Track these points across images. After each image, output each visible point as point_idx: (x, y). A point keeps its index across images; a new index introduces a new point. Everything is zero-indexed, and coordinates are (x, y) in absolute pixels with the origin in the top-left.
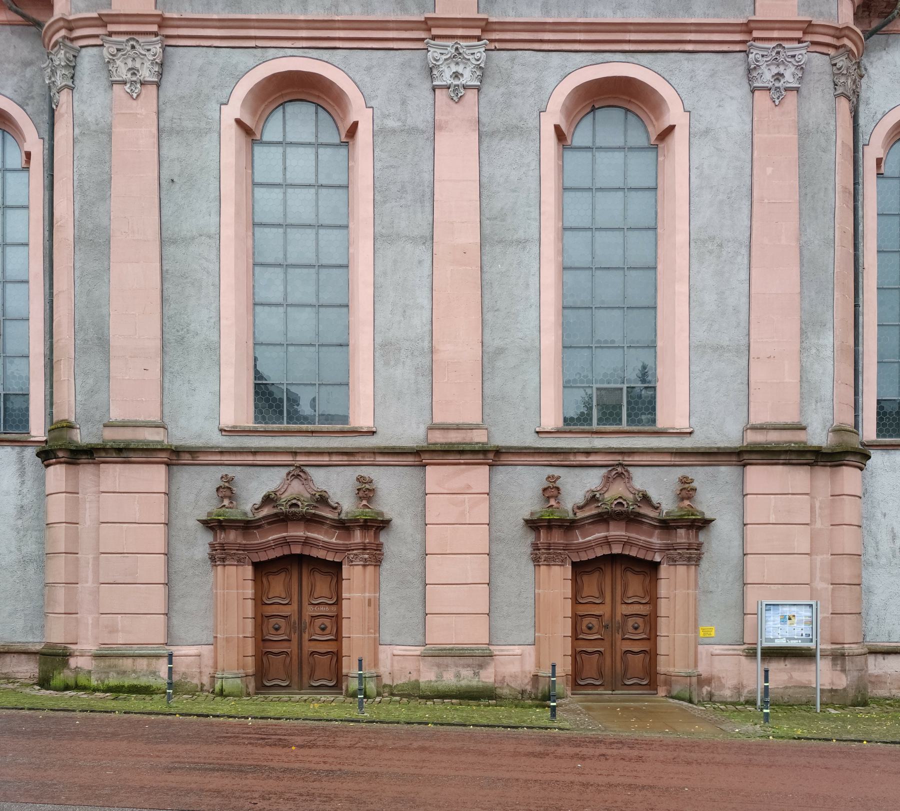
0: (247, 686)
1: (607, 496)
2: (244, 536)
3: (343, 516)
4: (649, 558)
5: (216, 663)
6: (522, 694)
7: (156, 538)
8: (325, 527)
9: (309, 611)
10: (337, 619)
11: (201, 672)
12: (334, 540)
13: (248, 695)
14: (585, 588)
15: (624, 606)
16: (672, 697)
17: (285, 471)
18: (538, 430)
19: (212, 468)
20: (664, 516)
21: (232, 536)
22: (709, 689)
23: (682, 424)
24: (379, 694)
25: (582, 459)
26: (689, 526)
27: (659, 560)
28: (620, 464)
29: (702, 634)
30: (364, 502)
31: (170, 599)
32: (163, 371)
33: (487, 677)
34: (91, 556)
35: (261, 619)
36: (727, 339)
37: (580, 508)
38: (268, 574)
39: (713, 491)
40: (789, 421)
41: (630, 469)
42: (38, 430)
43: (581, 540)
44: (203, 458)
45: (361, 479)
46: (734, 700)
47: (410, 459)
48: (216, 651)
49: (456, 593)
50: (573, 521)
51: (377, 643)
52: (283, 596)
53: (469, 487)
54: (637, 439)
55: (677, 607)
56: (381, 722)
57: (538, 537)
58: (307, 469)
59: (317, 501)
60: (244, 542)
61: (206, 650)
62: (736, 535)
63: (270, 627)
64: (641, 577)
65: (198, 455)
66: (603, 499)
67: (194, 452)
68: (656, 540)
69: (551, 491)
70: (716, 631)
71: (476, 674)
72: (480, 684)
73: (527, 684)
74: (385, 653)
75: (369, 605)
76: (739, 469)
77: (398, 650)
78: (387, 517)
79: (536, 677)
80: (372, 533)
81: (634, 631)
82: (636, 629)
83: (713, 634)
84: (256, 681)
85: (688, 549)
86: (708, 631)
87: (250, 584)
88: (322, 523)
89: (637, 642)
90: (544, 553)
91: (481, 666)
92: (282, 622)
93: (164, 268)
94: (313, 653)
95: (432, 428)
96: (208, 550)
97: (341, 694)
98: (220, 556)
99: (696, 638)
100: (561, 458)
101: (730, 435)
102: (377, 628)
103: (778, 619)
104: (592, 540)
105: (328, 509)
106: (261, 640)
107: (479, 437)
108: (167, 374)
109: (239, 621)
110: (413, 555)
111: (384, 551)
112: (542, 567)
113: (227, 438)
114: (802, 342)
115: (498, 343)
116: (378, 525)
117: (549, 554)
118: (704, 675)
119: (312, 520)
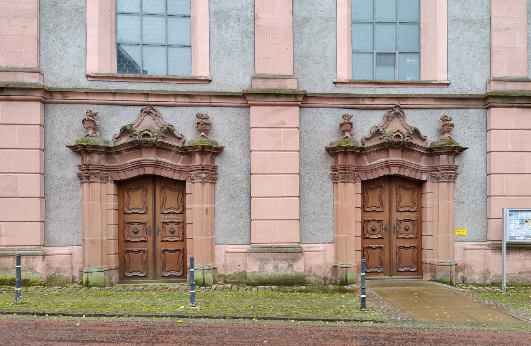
0: (110, 278)
1: (388, 131)
2: (107, 160)
3: (186, 145)
4: (418, 177)
6: (325, 280)
7: (33, 162)
8: (172, 154)
9: (161, 219)
10: (183, 224)
11: (72, 268)
12: (179, 164)
13: (112, 284)
14: (370, 200)
15: (398, 213)
16: (436, 281)
17: (139, 109)
18: (335, 81)
19: (80, 106)
20: (429, 146)
21: (96, 159)
22: (462, 274)
23: (442, 78)
24: (215, 282)
25: (368, 103)
27: (425, 179)
28: (398, 107)
29: (457, 234)
30: (203, 134)
31: (46, 210)
32: (40, 29)
33: (300, 268)
35: (123, 225)
36: (474, 15)
37: (367, 139)
38: (128, 190)
39: (466, 127)
41: (405, 111)
43: (368, 164)
44: (72, 98)
46: (482, 282)
47: (239, 101)
48: (83, 250)
49: (276, 202)
50: (363, 149)
51: (213, 243)
52: (141, 207)
53: (284, 123)
54: (409, 88)
55: (440, 214)
56: (209, 317)
57: (336, 161)
58: (157, 108)
59: (165, 133)
60: (107, 165)
61: (76, 250)
62: (482, 160)
63: (131, 231)
64: (411, 192)
65: (68, 95)
66: (385, 133)
67: (64, 93)
68: (423, 163)
69: (346, 126)
70: (467, 231)
71: (290, 266)
72: (294, 273)
73: (329, 273)
74: (220, 251)
75: (207, 213)
76: (484, 111)
78: (220, 145)
79: (335, 268)
80: (209, 157)
81: (405, 232)
82: (407, 230)
83: (465, 234)
84: (119, 273)
85: (448, 170)
86: (461, 231)
88: (170, 150)
89: (408, 240)
90: (341, 173)
91: (294, 260)
92: (140, 227)
94: (164, 251)
97: (186, 282)
98: (86, 174)
99: (454, 235)
100: (353, 102)
101: (477, 86)
102: (214, 232)
103: (518, 222)
104: (376, 164)
105: (174, 140)
106: (124, 242)
107: (291, 85)
108: (43, 31)
110: (241, 175)
111: (218, 172)
112: (339, 184)
113: (92, 83)
115: (305, 14)
116: (214, 151)
117: (346, 173)
119: (161, 148)
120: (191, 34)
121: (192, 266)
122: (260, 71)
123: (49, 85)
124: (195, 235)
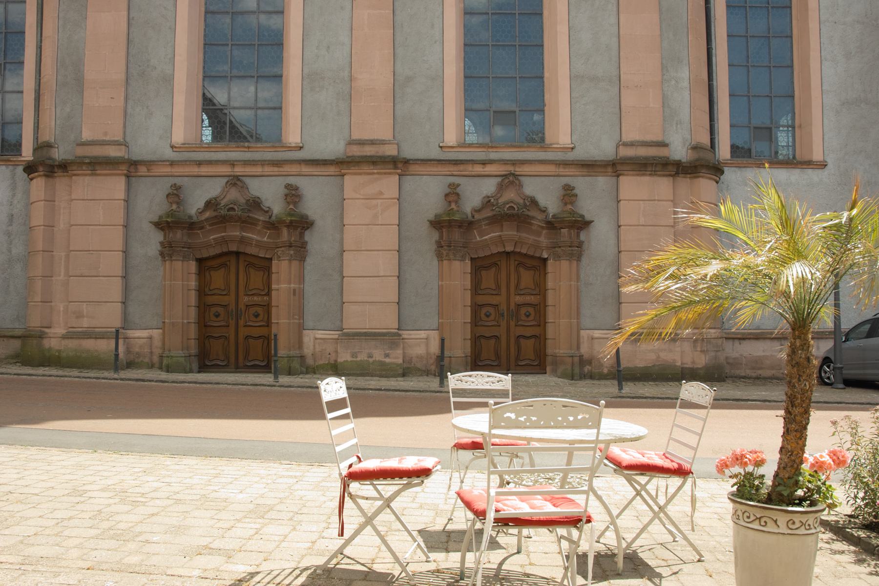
5: (164, 344)
10: (267, 307)
11: (151, 353)
22: (590, 368)
25: (478, 169)
26: (571, 226)
31: (126, 289)
32: (126, 99)
34: (63, 254)
37: (478, 211)
40: (655, 139)
42: (27, 153)
45: (288, 186)
47: (332, 170)
50: (471, 223)
51: (301, 328)
58: (244, 179)
61: (156, 333)
64: (532, 272)
66: (497, 203)
69: (453, 195)
74: (309, 337)
75: (294, 294)
77: (320, 334)
87: (193, 277)
93: (131, 17)
94: (247, 337)
95: (351, 143)
96: (160, 248)
98: (168, 251)
99: (578, 324)
102: (302, 316)
104: (488, 239)
106: (203, 324)
107: (390, 151)
109: (184, 310)
114: (663, 75)
118: (586, 356)
119: (247, 223)
120: (280, 95)
121: (276, 355)
122: (356, 136)
123: (135, 157)
124: (281, 321)
